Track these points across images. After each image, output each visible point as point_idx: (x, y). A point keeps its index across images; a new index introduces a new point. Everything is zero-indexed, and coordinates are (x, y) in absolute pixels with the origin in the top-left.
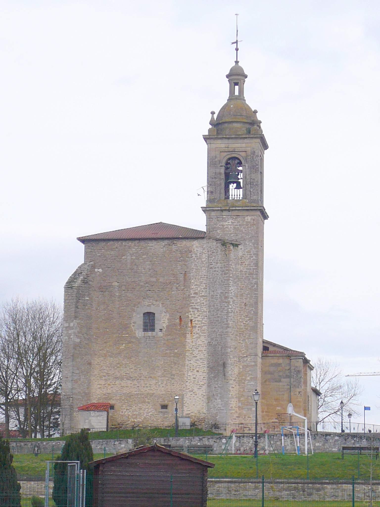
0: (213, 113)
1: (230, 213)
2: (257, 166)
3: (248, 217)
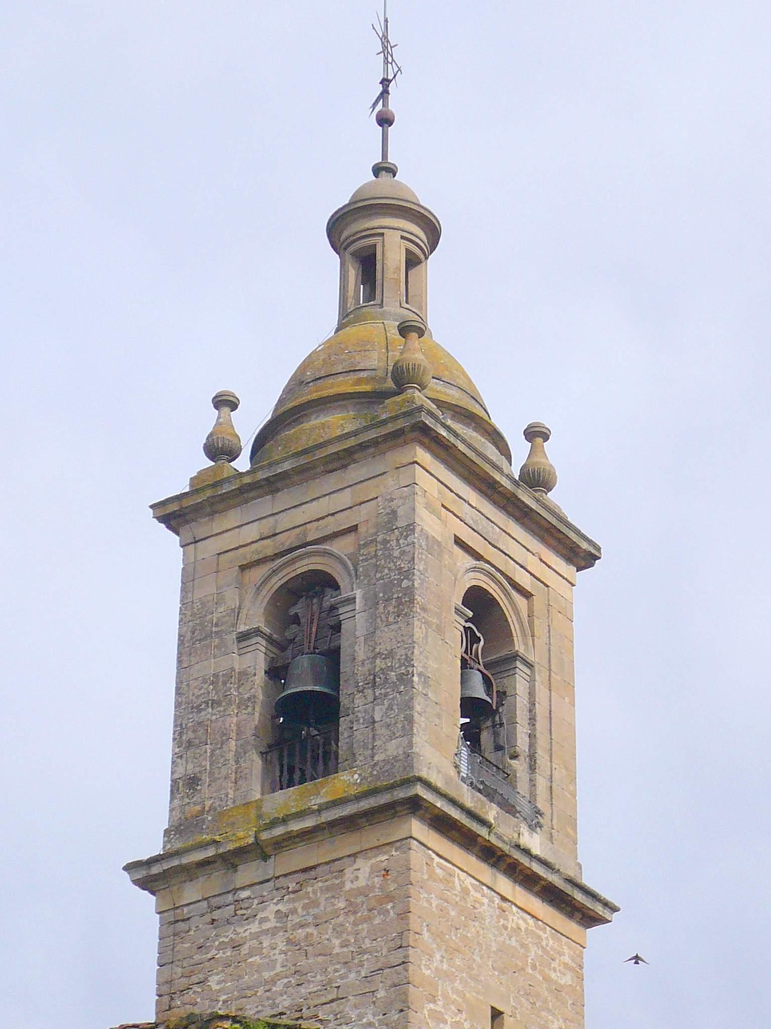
0: (225, 402)
1: (273, 867)
2: (405, 584)
3: (360, 863)
